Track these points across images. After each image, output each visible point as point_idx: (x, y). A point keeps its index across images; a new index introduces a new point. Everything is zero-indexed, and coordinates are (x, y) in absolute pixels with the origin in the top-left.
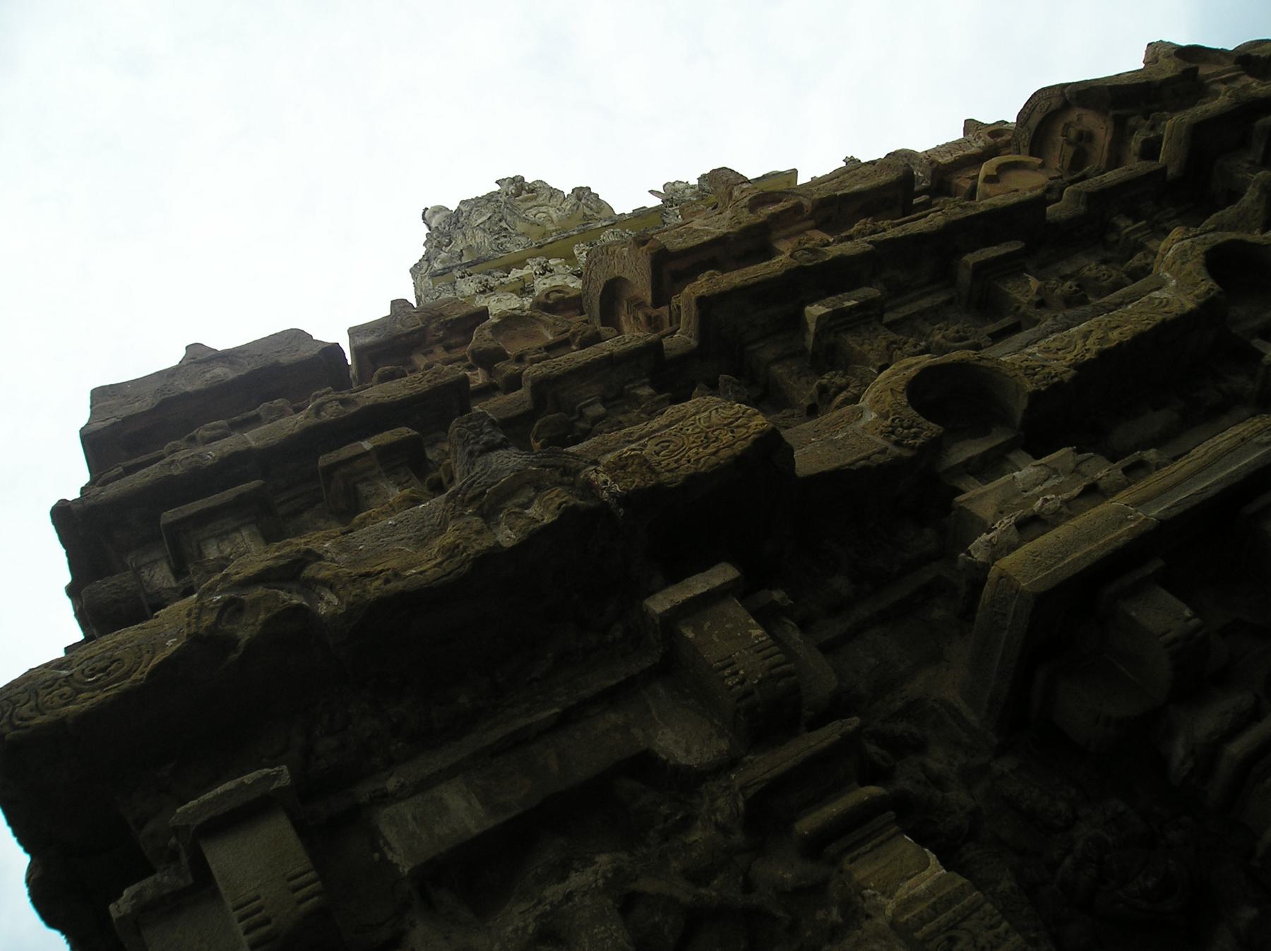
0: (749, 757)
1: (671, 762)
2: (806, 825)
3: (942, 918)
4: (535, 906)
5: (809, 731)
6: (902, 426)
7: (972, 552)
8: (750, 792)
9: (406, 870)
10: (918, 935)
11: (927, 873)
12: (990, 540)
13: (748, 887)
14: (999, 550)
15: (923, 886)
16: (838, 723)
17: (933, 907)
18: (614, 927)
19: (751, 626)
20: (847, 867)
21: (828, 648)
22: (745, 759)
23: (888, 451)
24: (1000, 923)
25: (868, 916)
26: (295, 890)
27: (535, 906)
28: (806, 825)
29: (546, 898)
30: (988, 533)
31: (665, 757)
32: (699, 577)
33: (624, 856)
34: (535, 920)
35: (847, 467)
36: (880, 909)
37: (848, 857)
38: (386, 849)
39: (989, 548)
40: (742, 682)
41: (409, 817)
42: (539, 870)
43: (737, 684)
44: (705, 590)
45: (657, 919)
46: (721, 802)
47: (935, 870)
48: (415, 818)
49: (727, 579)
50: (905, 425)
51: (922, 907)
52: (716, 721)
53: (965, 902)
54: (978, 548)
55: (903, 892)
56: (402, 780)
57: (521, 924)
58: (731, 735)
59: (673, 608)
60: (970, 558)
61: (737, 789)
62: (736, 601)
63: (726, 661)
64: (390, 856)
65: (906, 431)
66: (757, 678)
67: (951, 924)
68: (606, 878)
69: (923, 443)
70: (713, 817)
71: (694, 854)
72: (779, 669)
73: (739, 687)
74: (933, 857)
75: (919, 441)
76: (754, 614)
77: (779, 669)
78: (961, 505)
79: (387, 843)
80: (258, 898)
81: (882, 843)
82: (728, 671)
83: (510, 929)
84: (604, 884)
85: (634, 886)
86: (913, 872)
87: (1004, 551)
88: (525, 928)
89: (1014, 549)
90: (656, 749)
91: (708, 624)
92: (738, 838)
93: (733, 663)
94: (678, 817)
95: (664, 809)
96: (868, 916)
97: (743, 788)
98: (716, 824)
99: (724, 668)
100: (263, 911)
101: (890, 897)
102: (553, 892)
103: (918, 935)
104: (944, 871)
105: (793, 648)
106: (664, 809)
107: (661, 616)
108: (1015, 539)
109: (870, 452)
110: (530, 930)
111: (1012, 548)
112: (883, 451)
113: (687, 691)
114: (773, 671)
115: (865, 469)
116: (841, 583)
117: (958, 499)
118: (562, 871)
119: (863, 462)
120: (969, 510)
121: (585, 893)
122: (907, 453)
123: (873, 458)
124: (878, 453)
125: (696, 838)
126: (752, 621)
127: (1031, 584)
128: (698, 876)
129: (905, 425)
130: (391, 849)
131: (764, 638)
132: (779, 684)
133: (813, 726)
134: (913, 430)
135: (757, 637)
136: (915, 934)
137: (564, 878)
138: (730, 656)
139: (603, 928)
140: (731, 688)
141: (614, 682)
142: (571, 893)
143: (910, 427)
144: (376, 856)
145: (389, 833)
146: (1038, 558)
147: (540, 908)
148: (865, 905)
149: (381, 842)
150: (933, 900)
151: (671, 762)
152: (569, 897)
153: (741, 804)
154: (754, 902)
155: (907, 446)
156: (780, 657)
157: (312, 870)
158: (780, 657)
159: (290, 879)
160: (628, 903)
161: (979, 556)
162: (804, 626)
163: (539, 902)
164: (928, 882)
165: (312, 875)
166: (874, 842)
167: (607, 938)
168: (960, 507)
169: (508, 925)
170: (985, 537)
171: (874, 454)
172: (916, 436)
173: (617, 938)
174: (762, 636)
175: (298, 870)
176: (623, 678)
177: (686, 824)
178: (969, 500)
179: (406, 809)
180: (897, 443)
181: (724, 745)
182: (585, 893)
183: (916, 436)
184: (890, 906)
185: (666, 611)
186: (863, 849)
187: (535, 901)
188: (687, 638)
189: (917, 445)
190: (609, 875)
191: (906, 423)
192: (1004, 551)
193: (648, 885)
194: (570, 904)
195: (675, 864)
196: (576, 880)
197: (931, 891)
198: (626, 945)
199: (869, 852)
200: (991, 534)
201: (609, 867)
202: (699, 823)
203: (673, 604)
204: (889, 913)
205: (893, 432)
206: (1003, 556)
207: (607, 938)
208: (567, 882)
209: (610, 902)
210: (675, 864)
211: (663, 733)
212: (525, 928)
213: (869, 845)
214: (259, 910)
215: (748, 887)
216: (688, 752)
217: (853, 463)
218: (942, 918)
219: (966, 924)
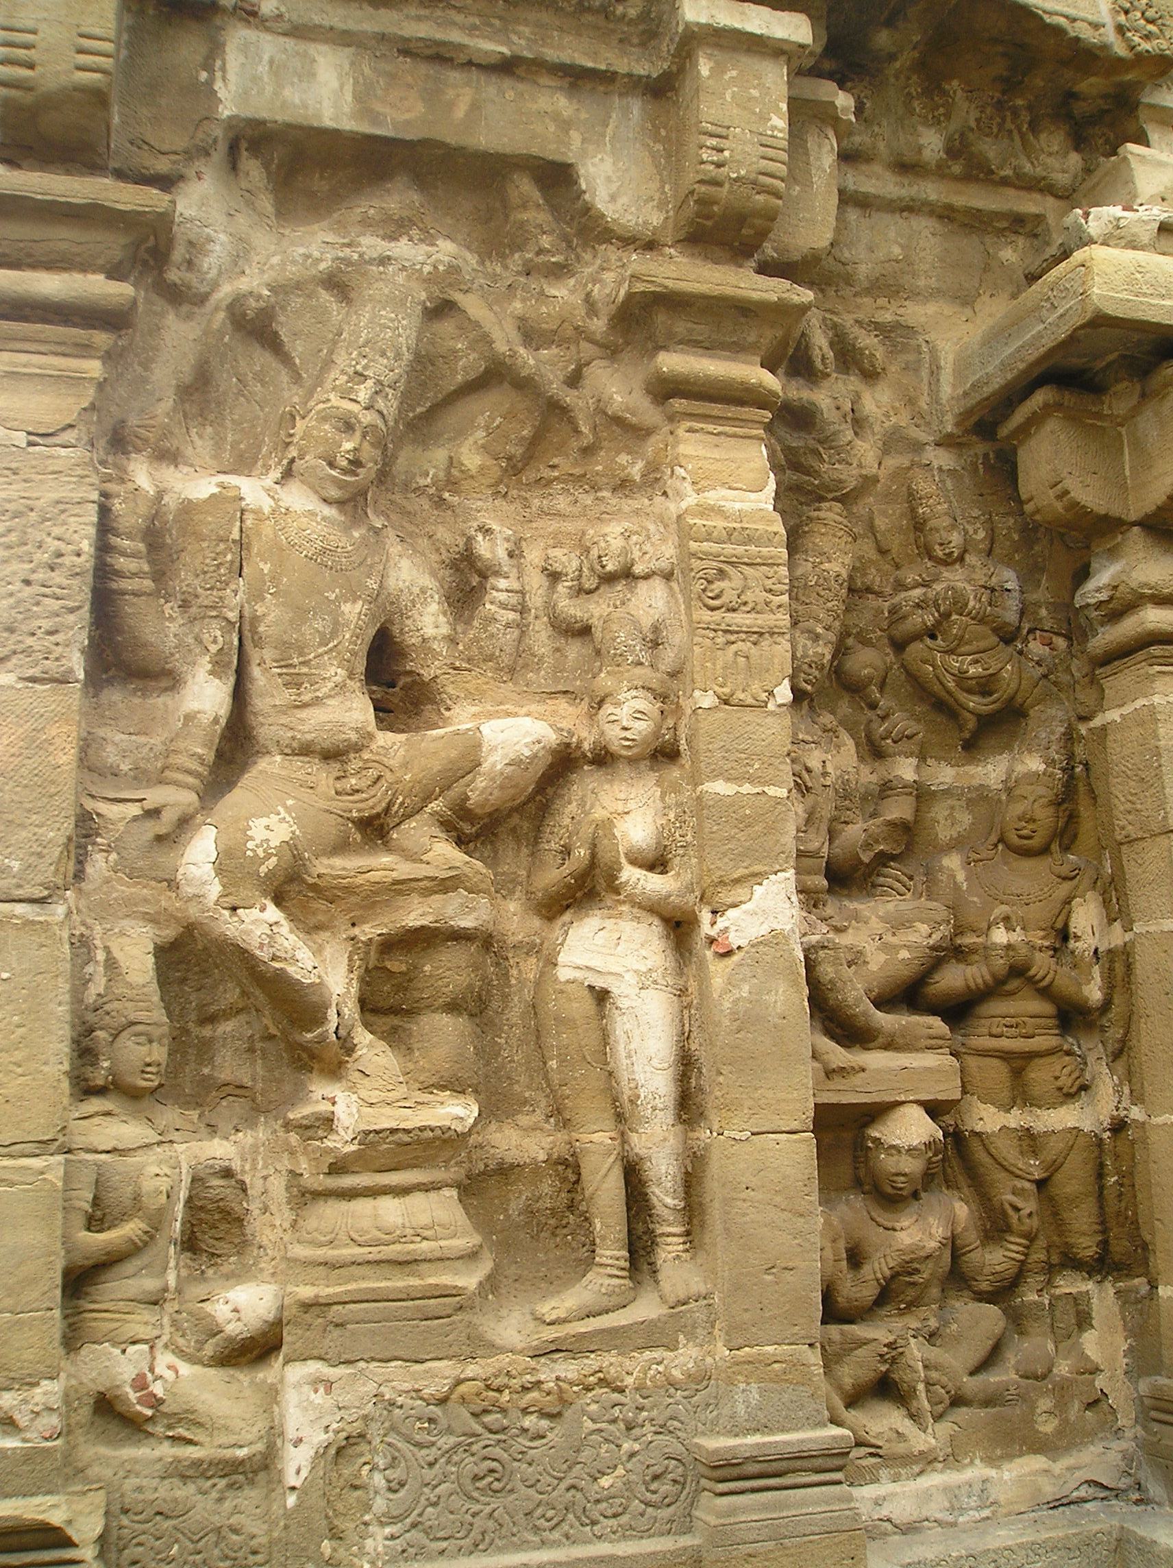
0: (672, 250)
1: (587, 197)
2: (673, 362)
3: (729, 549)
4: (344, 245)
5: (758, 272)
6: (1143, 14)
7: (1091, 217)
8: (640, 287)
9: (227, 113)
10: (693, 546)
11: (753, 496)
12: (1119, 219)
13: (574, 380)
14: (1117, 237)
15: (738, 506)
16: (786, 284)
17: (730, 533)
18: (404, 322)
19: (777, 110)
20: (681, 432)
21: (847, 199)
22: (667, 250)
23: (1102, 30)
24: (782, 594)
25: (665, 494)
26: (81, 51)
27: (344, 245)
28: (673, 362)
29: (360, 245)
30: (1124, 210)
31: (584, 187)
32: (765, 11)
33: (472, 259)
34: (333, 260)
35: (1040, 12)
36: (680, 495)
37: (689, 424)
38: (218, 74)
39: (1110, 226)
40: (719, 165)
41: (266, 57)
42: (372, 211)
43: (712, 163)
44: (759, 32)
45: (460, 346)
46: (609, 276)
47: (765, 499)
48: (271, 62)
49: (793, 38)
50: (1147, 14)
51: (721, 524)
52: (667, 188)
53: (765, 550)
54: (1100, 218)
55: (713, 497)
56: (283, 9)
57: (316, 254)
58: (671, 213)
59: (709, 26)
60: (1083, 221)
61: (629, 273)
62: (785, 70)
63: (720, 129)
64: (218, 85)
65: (1142, 22)
66: (739, 173)
67: (734, 559)
68: (435, 267)
69: (1147, 51)
70: (590, 285)
71: (544, 309)
72: (768, 180)
73: (712, 167)
74: (772, 486)
75: (1145, 46)
76: (793, 102)
77: (768, 180)
78: (1129, 156)
79: (223, 69)
80: (34, 32)
81: (734, 436)
82: (713, 142)
83: (302, 250)
84: (429, 273)
85: (458, 297)
86: (740, 485)
87: (1123, 242)
88: (318, 261)
89: (1134, 248)
90: (582, 172)
91: (734, 73)
92: (599, 325)
93: (726, 138)
94: (553, 260)
95: (546, 241)
96: (665, 494)
97: (635, 277)
98: (588, 295)
99: (712, 135)
100: (33, 51)
101: (698, 492)
102: (371, 244)
103: (693, 546)
104: (771, 508)
105: (813, 172)
106: (546, 241)
107: (687, 25)
108: (1145, 238)
109: (1082, 14)
110: (322, 266)
111: (1133, 245)
112: (1096, 26)
113: (663, 133)
114: (763, 179)
115: (1058, 31)
116: (932, 143)
117: (1131, 147)
118: (396, 228)
119: (1062, 21)
120: (1132, 170)
121: (404, 268)
122: (1120, 50)
123: (1078, 24)
124: (1090, 24)
125: (557, 294)
126: (784, 107)
127: (1105, 296)
128: (531, 335)
129: (1147, 14)
130: (224, 79)
131: (781, 135)
132: (758, 197)
133: (765, 269)
134: (1151, 27)
135: (774, 128)
136: (691, 542)
137: (393, 238)
138: (728, 128)
139: (393, 315)
140: (703, 163)
141: (590, 65)
142: (389, 258)
143: (1151, 21)
144: (204, 76)
145: (233, 59)
146: (1138, 276)
147: (347, 250)
148: (669, 482)
149: (218, 63)
150: (735, 525)
151: (587, 197)
152: (384, 261)
153: (622, 293)
154: (568, 399)
155: (1128, 40)
156: (782, 169)
157: (111, 41)
158: (782, 169)
159: (82, 36)
160: (441, 310)
161: (1094, 227)
162: (847, 157)
163: (349, 245)
164: (746, 506)
165: (108, 47)
166: (727, 429)
167: (389, 328)
168: (1125, 158)
169: (302, 245)
170: (1117, 211)
171: (1083, 20)
172: (1147, 37)
173: (399, 335)
174: (781, 131)
175: (97, 31)
176: (603, 67)
177: (558, 272)
178: (1142, 158)
179: (269, 45)
180: (1120, 29)
181: (656, 219)
182: (404, 268)
183: (1147, 37)
184: (691, 500)
185: (698, 24)
186: (710, 427)
187: (346, 241)
188: (699, 72)
189: (1139, 48)
190: (441, 268)
191: (1150, 13)
192: (1123, 242)
193: (472, 305)
194: (381, 268)
195: (518, 305)
196: (403, 248)
197: (741, 516)
198: (404, 349)
199: (712, 434)
200: (1126, 214)
201: (446, 259)
202: (572, 282)
203: (711, 22)
204: (684, 505)
205: (1126, 12)
206: (1116, 246)
207: (389, 328)
208: (393, 244)
209: (423, 296)
210: (518, 305)
211: (602, 160)
212: (318, 261)
213: (720, 429)
214: (27, 47)
215: (574, 380)
216: (613, 198)
217: (1050, 13)
218: (729, 549)
219: (748, 571)
